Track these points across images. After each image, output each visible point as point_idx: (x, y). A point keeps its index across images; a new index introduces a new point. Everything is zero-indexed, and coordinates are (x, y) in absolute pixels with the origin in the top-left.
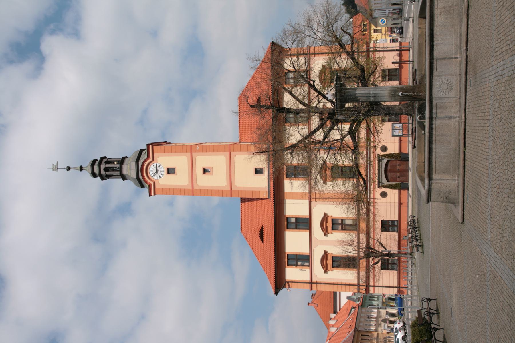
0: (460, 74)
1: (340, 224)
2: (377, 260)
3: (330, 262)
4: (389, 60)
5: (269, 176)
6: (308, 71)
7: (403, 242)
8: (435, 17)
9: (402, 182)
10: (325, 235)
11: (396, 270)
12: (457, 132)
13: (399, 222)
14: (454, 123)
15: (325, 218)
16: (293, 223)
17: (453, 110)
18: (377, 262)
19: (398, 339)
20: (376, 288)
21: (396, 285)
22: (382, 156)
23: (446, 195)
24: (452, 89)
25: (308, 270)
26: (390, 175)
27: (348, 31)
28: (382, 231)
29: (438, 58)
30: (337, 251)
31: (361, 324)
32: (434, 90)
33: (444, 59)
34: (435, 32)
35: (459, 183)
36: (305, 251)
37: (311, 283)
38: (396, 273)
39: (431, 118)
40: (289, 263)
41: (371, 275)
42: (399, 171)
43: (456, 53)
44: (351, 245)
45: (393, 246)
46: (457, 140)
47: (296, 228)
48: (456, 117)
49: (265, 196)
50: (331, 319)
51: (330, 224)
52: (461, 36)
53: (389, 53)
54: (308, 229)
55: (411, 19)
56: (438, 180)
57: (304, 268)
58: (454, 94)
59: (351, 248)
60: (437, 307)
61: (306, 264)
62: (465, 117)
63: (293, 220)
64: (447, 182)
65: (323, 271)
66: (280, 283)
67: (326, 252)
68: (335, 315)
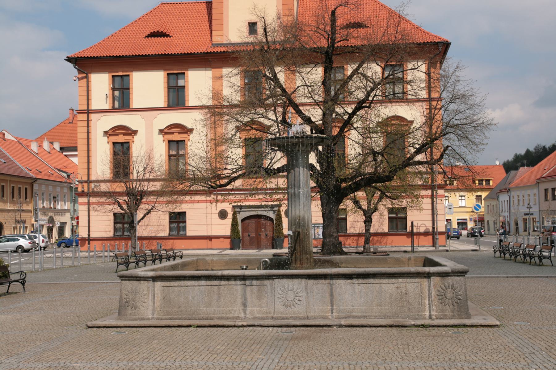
0: (308, 318)
1: (178, 152)
2: (125, 207)
3: (121, 139)
4: (419, 218)
5: (247, 43)
6: (403, 99)
7: (155, 242)
8: (393, 280)
9: (243, 240)
10: (161, 131)
11: (114, 235)
12: (224, 315)
13: (184, 237)
14: (237, 310)
15: (186, 130)
16: (177, 83)
17: (255, 309)
18: (122, 208)
19: (18, 240)
20: (87, 207)
21: (93, 235)
22: (279, 211)
23: (131, 302)
24: (287, 307)
25: (107, 106)
26: (252, 222)
27: (445, 156)
28: (171, 214)
29: (334, 286)
30: (138, 149)
31: (43, 188)
32: (285, 281)
33: (332, 295)
34: (372, 281)
35: (149, 319)
36: (136, 102)
37: (88, 112)
38: (111, 234)
39: (244, 278)
40: (116, 78)
41: (103, 200)
42: (258, 235)
43: (339, 311)
44: (145, 169)
45: (148, 229)
46: (212, 315)
47: (169, 88)
48: (245, 313)
49: (217, 39)
50: (52, 143)
51: (177, 137)
52: (364, 317)
53: (430, 218)
54: (168, 105)
55: (477, 248)
56: (154, 290)
57: (110, 101)
58: (279, 309)
59: (141, 169)
60: (11, 293)
61: (117, 104)
62: (243, 326)
63: (181, 83)
64: (150, 303)
65: (107, 129)
66: (85, 64)
67: (135, 132)
68: (58, 149)
